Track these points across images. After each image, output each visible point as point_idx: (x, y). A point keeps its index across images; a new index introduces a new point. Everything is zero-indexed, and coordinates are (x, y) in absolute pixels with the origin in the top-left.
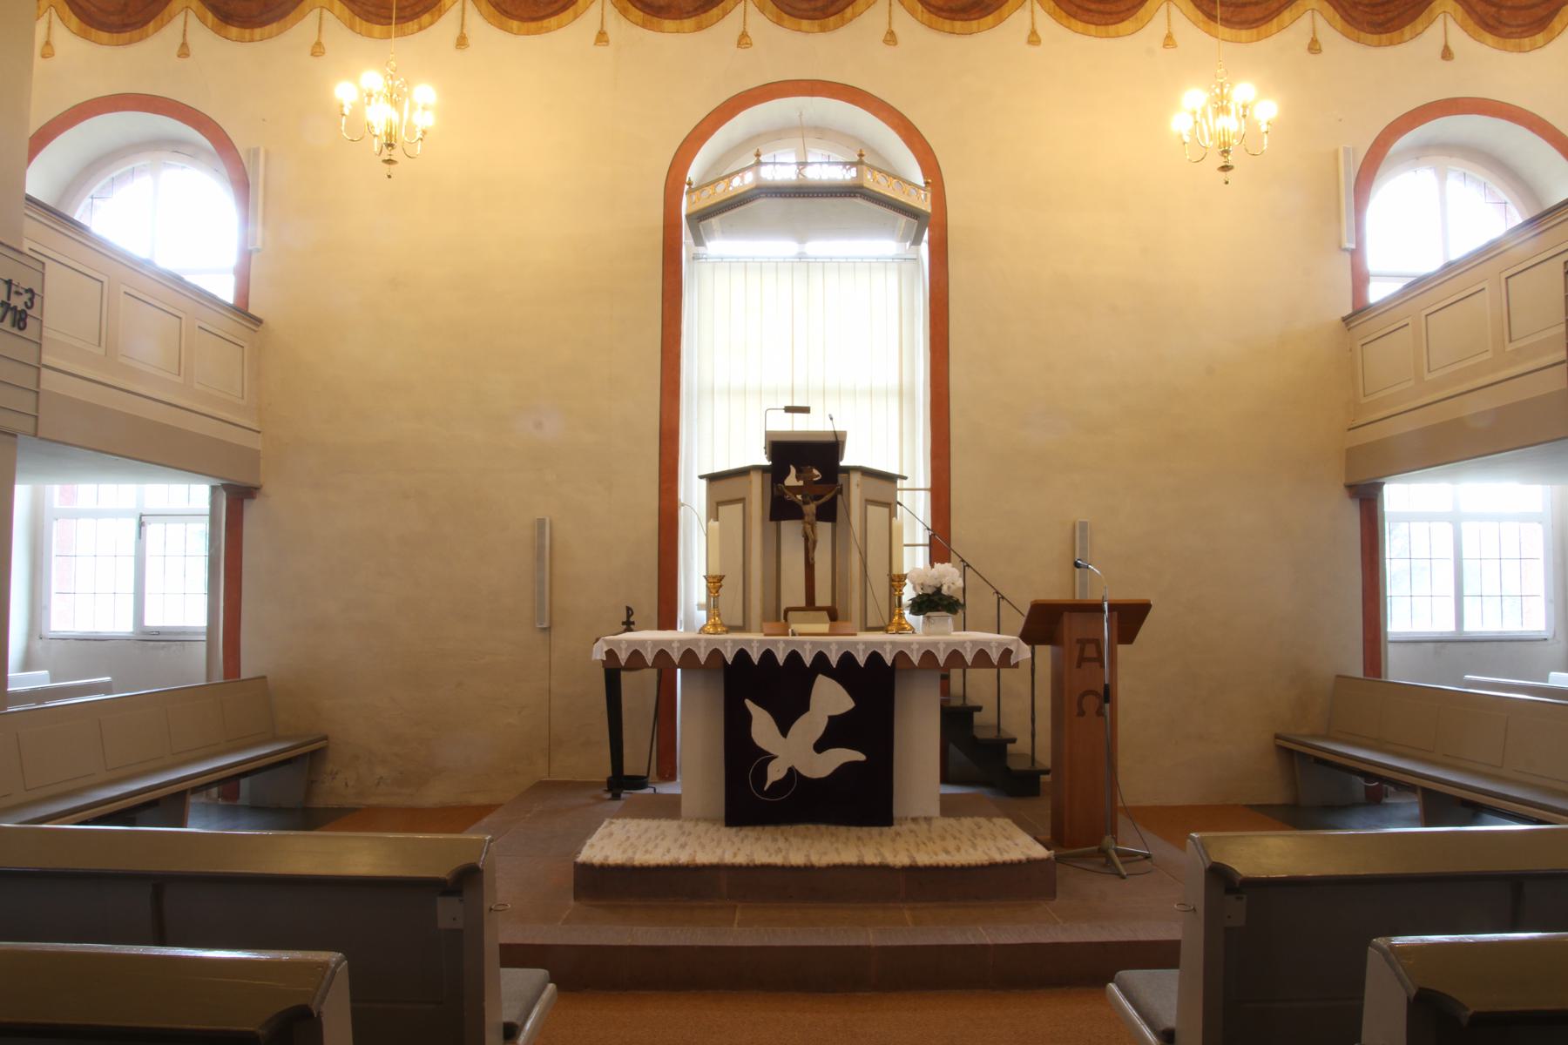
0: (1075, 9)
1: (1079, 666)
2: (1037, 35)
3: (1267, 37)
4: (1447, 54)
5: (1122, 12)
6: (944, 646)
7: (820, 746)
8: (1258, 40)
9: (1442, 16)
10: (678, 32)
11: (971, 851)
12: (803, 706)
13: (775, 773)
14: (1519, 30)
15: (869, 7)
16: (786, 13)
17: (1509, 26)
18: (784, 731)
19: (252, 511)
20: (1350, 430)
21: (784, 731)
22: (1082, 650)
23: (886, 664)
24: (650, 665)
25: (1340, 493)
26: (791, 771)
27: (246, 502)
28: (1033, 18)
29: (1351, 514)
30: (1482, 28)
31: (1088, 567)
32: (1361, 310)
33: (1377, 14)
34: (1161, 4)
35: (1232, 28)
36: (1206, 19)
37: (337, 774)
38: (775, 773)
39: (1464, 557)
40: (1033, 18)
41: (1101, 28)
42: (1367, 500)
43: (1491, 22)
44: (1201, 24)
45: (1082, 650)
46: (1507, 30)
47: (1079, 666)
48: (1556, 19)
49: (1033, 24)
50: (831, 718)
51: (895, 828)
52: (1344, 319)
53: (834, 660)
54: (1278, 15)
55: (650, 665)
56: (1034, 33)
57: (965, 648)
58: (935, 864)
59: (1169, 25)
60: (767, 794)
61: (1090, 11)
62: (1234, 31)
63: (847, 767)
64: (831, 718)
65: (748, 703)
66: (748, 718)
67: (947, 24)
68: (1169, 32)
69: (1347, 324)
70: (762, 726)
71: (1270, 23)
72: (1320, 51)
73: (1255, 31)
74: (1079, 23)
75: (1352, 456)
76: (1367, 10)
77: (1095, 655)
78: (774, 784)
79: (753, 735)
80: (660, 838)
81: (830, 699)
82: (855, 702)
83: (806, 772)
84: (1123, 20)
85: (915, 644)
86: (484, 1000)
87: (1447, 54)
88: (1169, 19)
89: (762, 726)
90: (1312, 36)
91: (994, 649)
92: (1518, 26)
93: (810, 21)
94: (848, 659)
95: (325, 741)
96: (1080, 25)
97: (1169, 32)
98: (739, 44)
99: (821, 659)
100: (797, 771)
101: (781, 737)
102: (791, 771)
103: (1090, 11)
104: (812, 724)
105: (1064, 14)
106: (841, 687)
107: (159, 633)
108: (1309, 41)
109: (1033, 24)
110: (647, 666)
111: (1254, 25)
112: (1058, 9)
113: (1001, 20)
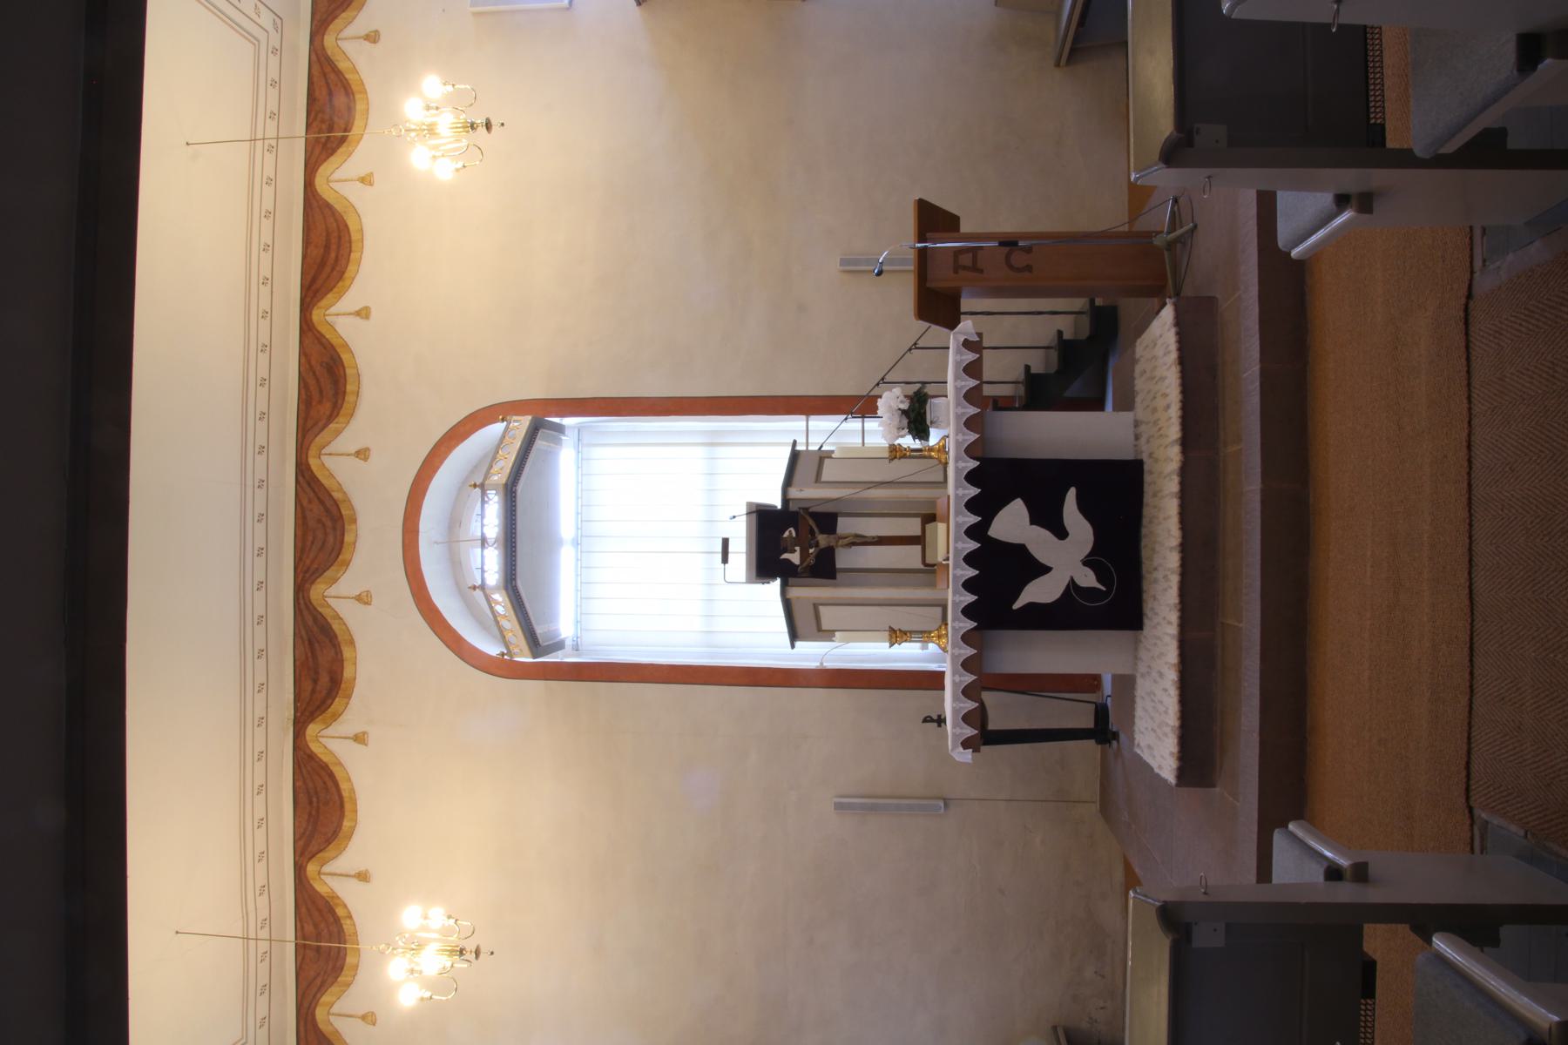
6: (960, 408)
7: (1061, 533)
12: (1021, 550)
13: (1088, 579)
18: (1045, 570)
21: (1045, 570)
23: (976, 575)
24: (978, 356)
26: (1086, 563)
37: (1091, 1018)
47: (981, 271)
50: (1032, 523)
51: (1145, 457)
55: (978, 356)
58: (1180, 420)
63: (1083, 507)
64: (1032, 523)
65: (1016, 606)
66: (1031, 607)
67: (349, 398)
70: (1041, 592)
71: (351, 82)
72: (377, 32)
74: (349, 268)
78: (1099, 580)
81: (1013, 523)
89: (1041, 592)
93: (346, 534)
94: (972, 505)
95: (1058, 1029)
96: (351, 268)
98: (367, 603)
99: (972, 532)
102: (1086, 563)
103: (337, 257)
104: (1038, 542)
105: (340, 284)
113: (346, 345)
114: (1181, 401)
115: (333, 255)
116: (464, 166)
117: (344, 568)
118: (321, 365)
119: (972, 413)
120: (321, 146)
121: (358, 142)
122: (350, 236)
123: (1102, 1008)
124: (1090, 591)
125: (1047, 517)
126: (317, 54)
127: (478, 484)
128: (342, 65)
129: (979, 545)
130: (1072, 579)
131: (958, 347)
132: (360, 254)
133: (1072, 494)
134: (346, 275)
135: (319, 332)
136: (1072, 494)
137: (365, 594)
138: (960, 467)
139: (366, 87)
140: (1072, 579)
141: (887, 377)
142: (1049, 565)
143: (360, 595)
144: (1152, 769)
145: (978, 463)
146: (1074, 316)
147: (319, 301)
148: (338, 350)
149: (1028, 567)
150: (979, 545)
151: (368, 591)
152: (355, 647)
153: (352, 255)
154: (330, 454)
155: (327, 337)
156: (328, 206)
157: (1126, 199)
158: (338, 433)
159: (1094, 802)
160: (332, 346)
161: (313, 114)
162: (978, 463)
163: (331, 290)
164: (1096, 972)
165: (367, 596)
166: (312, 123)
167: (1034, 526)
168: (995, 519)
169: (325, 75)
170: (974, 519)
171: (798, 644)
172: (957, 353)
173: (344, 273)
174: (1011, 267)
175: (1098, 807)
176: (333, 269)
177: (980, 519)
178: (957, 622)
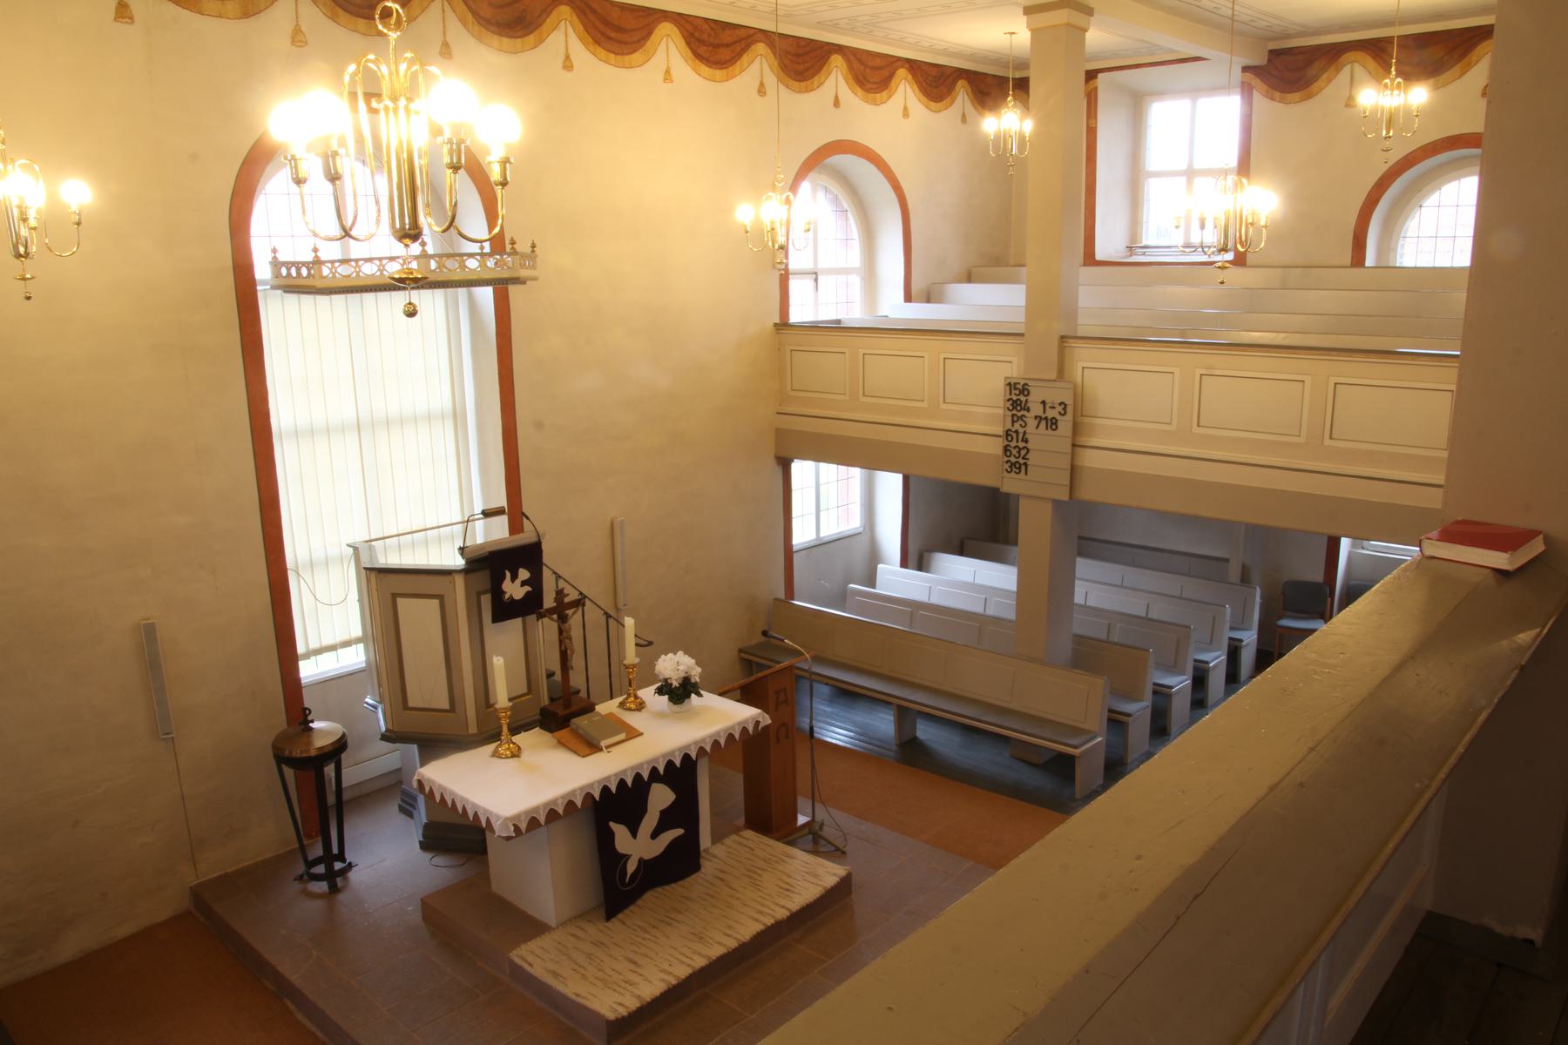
0: (599, 35)
2: (571, 62)
3: (733, 78)
4: (837, 103)
5: (634, 43)
7: (654, 835)
8: (727, 80)
9: (835, 70)
10: (220, 17)
11: (556, 675)
12: (643, 810)
14: (875, 86)
15: (423, 11)
16: (341, 7)
17: (870, 83)
20: (779, 413)
25: (771, 462)
28: (566, 41)
29: (779, 472)
30: (790, 77)
31: (783, 641)
32: (783, 325)
33: (799, 63)
34: (662, 39)
35: (710, 67)
36: (694, 58)
39: (971, 580)
40: (566, 41)
41: (619, 58)
42: (785, 465)
43: (861, 78)
44: (690, 62)
46: (869, 86)
48: (893, 81)
49: (567, 50)
50: (661, 812)
52: (775, 325)
54: (739, 58)
56: (668, 72)
59: (668, 61)
61: (610, 38)
62: (711, 70)
66: (612, 834)
68: (668, 67)
69: (778, 330)
71: (733, 66)
72: (765, 93)
73: (725, 71)
74: (603, 51)
75: (781, 434)
76: (793, 59)
79: (617, 847)
80: (584, 972)
81: (661, 797)
82: (673, 790)
83: (646, 857)
84: (634, 51)
87: (837, 103)
88: (668, 55)
90: (295, 23)
92: (874, 83)
93: (366, 21)
96: (603, 53)
97: (668, 67)
98: (293, 41)
103: (610, 38)
104: (650, 821)
105: (590, 40)
106: (669, 790)
108: (758, 84)
109: (567, 50)
110: (541, 826)
111: (725, 66)
112: (586, 35)
113: (541, 41)
114: (811, 903)
115: (613, 35)
116: (747, 232)
117: (329, 15)
118: (524, 10)
120: (692, 31)
121: (694, 70)
122: (628, 54)
126: (753, 35)
127: (515, 246)
128: (745, 58)
130: (631, 856)
132: (613, 63)
134: (597, 46)
135: (551, 12)
137: (304, 40)
139: (731, 81)
140: (631, 856)
141: (561, 580)
143: (302, 32)
146: (816, 803)
147: (577, 15)
148: (537, 31)
151: (306, 42)
152: (241, 18)
153: (613, 55)
154: (443, 10)
155: (548, 20)
156: (649, 34)
158: (464, 23)
159: (197, 876)
160: (540, 25)
161: (714, 26)
163: (586, 30)
165: (301, 41)
166: (707, 23)
167: (658, 814)
169: (739, 41)
171: (364, 571)
173: (599, 44)
175: (195, 883)
176: (602, 34)
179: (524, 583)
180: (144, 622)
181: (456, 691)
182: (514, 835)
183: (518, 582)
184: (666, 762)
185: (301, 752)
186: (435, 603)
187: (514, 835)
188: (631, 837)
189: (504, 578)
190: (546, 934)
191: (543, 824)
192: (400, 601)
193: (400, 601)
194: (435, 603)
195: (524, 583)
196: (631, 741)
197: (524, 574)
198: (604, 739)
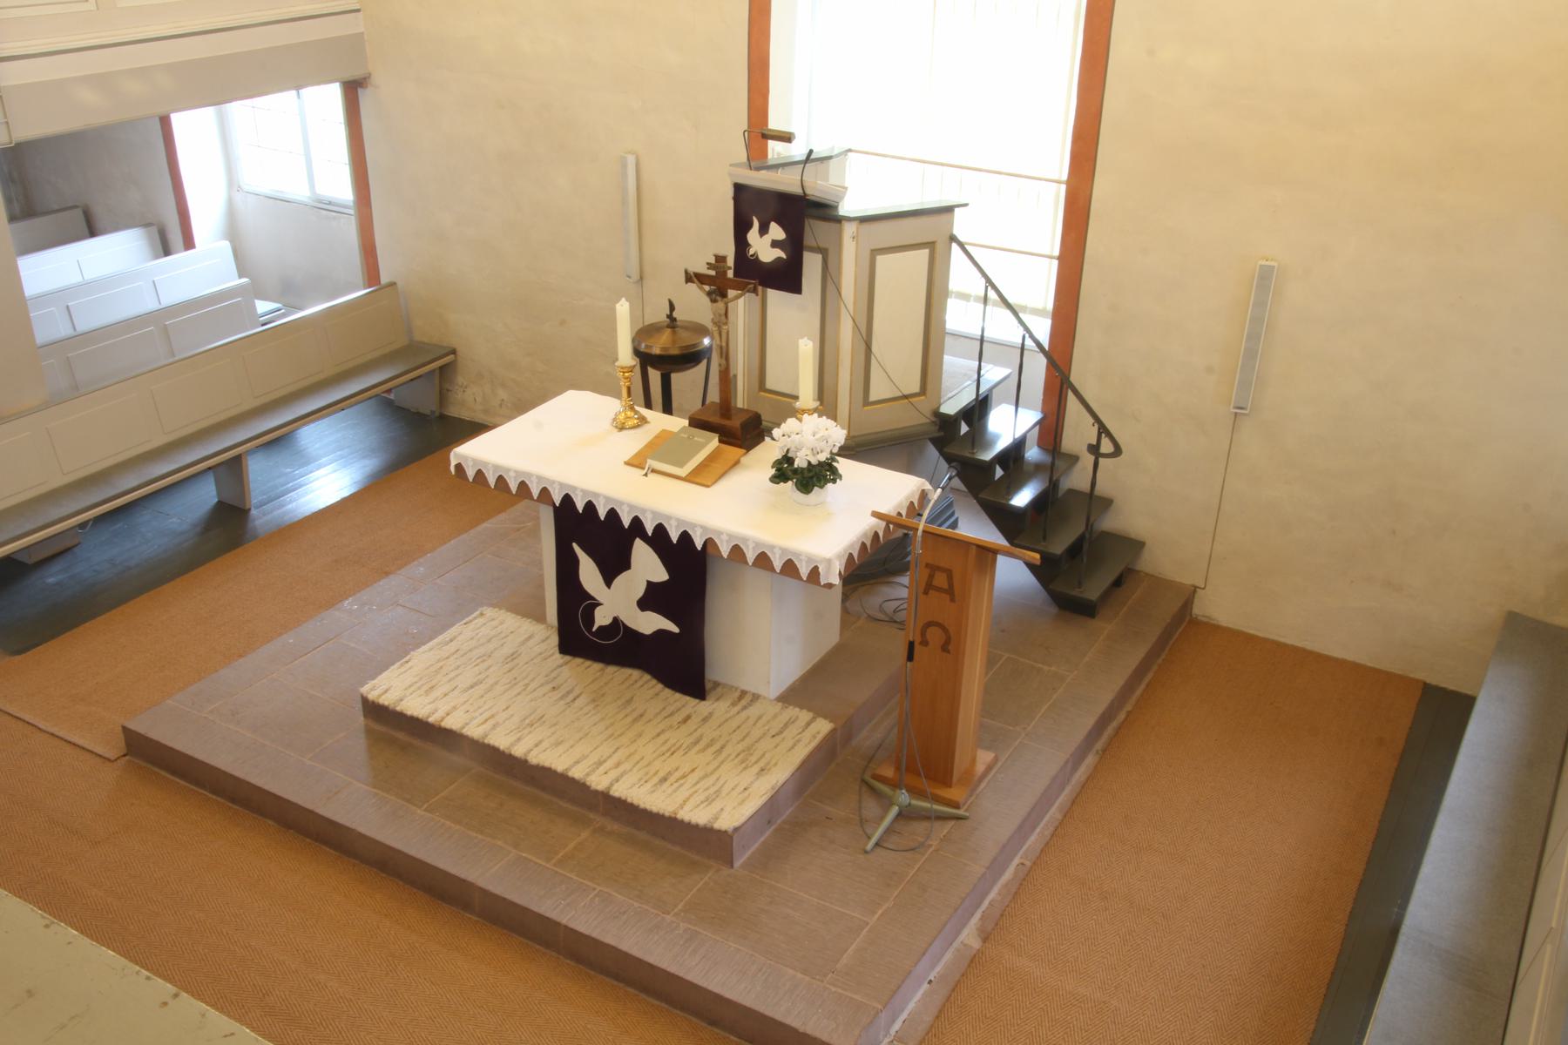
1: (926, 592)
6: (754, 545)
11: (1079, 465)
12: (625, 564)
13: (602, 618)
18: (608, 583)
19: (366, 99)
21: (608, 583)
22: (931, 577)
26: (616, 620)
27: (360, 91)
37: (466, 387)
38: (602, 618)
45: (931, 577)
47: (926, 592)
50: (649, 583)
51: (703, 707)
53: (650, 530)
57: (774, 554)
58: (623, 798)
60: (593, 634)
63: (661, 633)
64: (649, 583)
70: (589, 574)
77: (946, 586)
78: (601, 628)
81: (647, 566)
82: (669, 574)
85: (725, 535)
86: (1043, 400)
89: (589, 574)
91: (804, 563)
95: (452, 356)
100: (623, 624)
101: (604, 585)
102: (616, 620)
107: (330, 203)
119: (747, 556)
123: (475, 400)
124: (589, 618)
125: (652, 599)
129: (626, 527)
131: (816, 561)
133: (675, 629)
136: (675, 629)
138: (696, 529)
140: (602, 604)
142: (613, 585)
144: (373, 679)
145: (699, 549)
149: (614, 565)
150: (626, 527)
157: (1289, 641)
162: (699, 549)
164: (503, 400)
168: (651, 550)
170: (650, 530)
172: (809, 558)
174: (929, 624)
177: (650, 535)
178: (558, 487)
179: (775, 244)
180: (1264, 262)
181: (827, 368)
182: (805, 579)
183: (768, 238)
184: (585, 502)
185: (647, 346)
186: (880, 259)
187: (805, 579)
188: (606, 588)
189: (750, 226)
190: (529, 620)
191: (750, 564)
192: (925, 252)
193: (925, 252)
194: (880, 259)
195: (775, 244)
196: (687, 483)
197: (777, 232)
198: (652, 459)
